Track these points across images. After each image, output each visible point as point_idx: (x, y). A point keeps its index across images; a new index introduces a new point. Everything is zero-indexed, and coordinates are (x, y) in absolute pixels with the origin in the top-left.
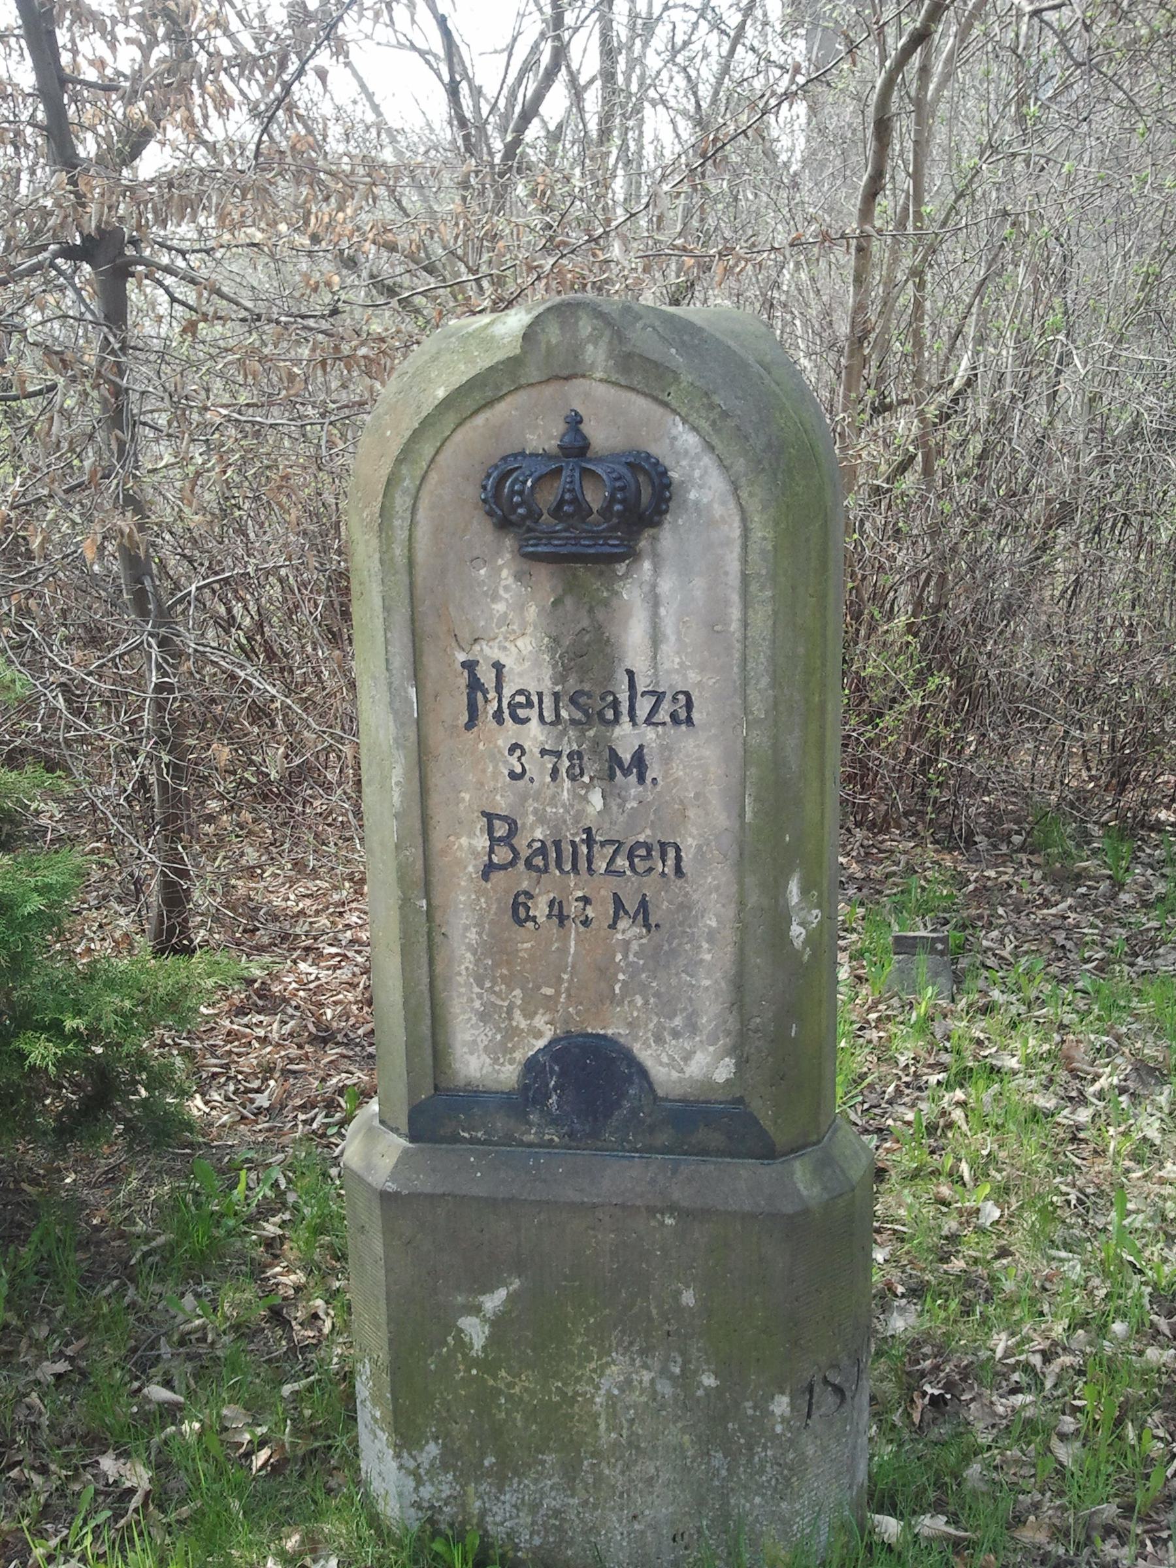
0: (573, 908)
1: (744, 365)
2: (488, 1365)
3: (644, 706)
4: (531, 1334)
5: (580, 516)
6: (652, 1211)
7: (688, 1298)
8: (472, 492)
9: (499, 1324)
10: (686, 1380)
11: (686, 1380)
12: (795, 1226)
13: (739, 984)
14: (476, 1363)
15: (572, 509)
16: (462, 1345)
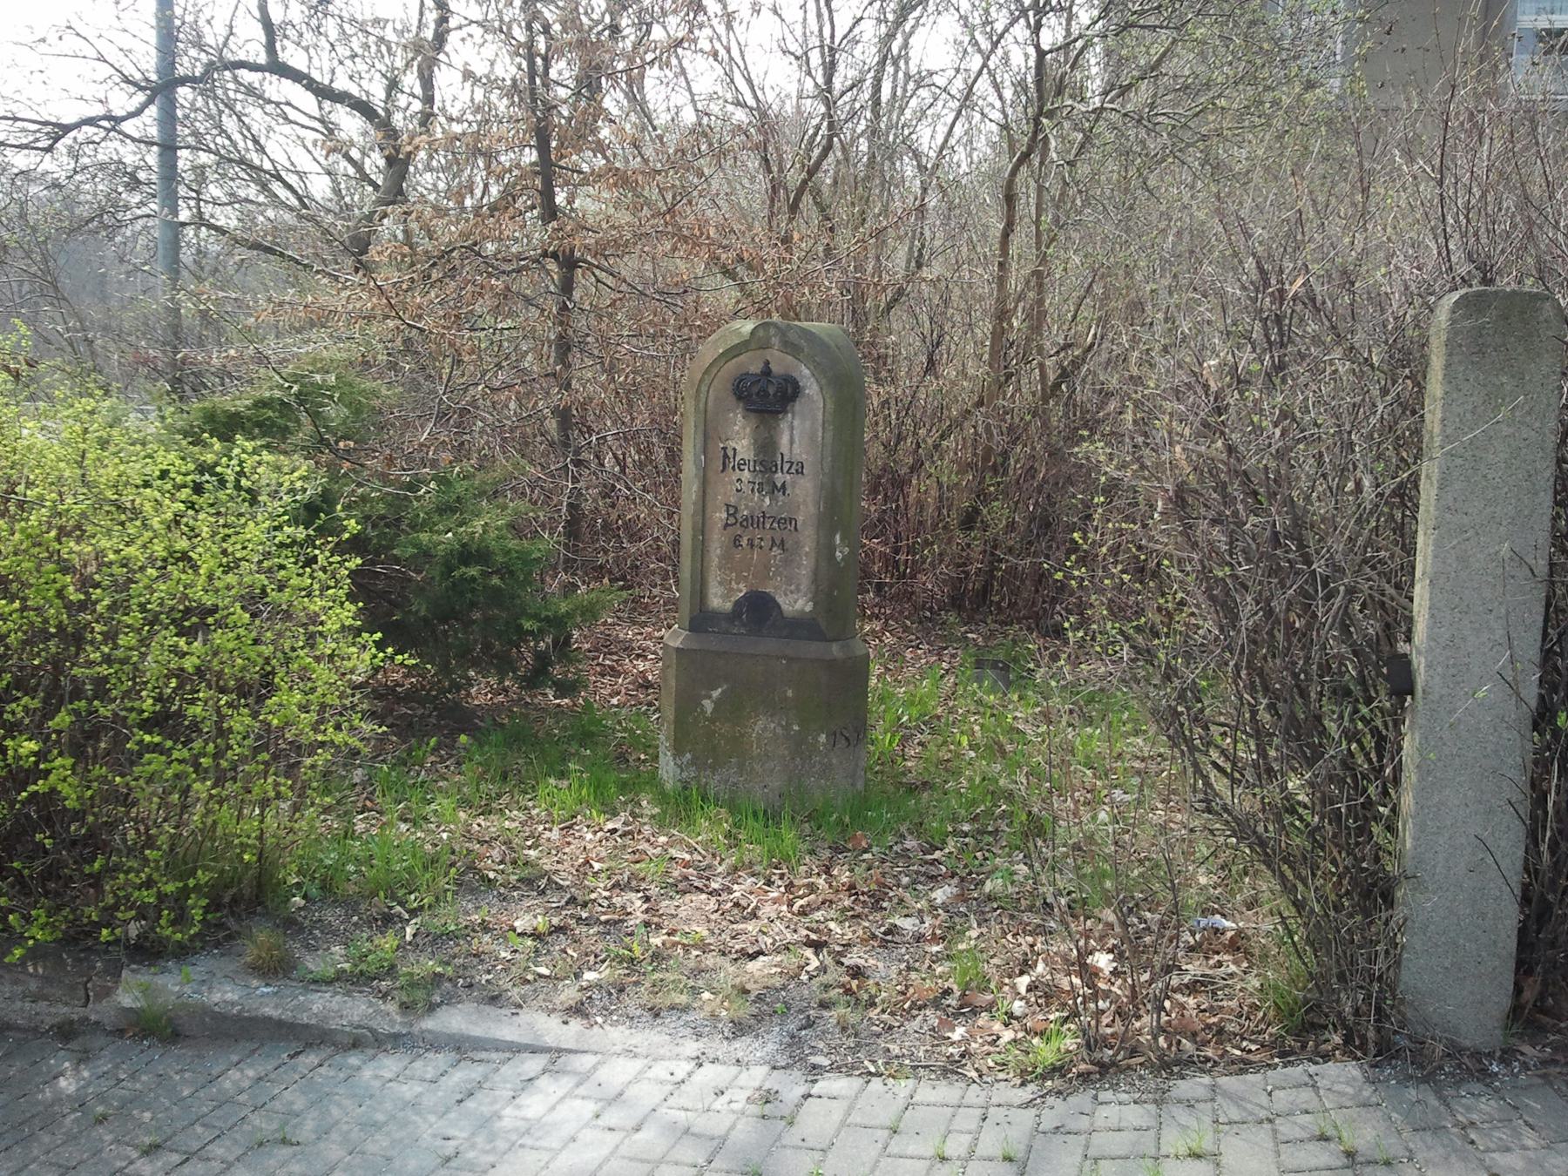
0: (757, 542)
1: (829, 347)
2: (712, 721)
3: (786, 467)
4: (732, 709)
5: (767, 397)
6: (778, 658)
7: (790, 693)
8: (730, 386)
9: (718, 703)
10: (787, 728)
11: (787, 728)
12: (831, 665)
13: (816, 572)
14: (707, 719)
15: (763, 394)
16: (703, 712)
